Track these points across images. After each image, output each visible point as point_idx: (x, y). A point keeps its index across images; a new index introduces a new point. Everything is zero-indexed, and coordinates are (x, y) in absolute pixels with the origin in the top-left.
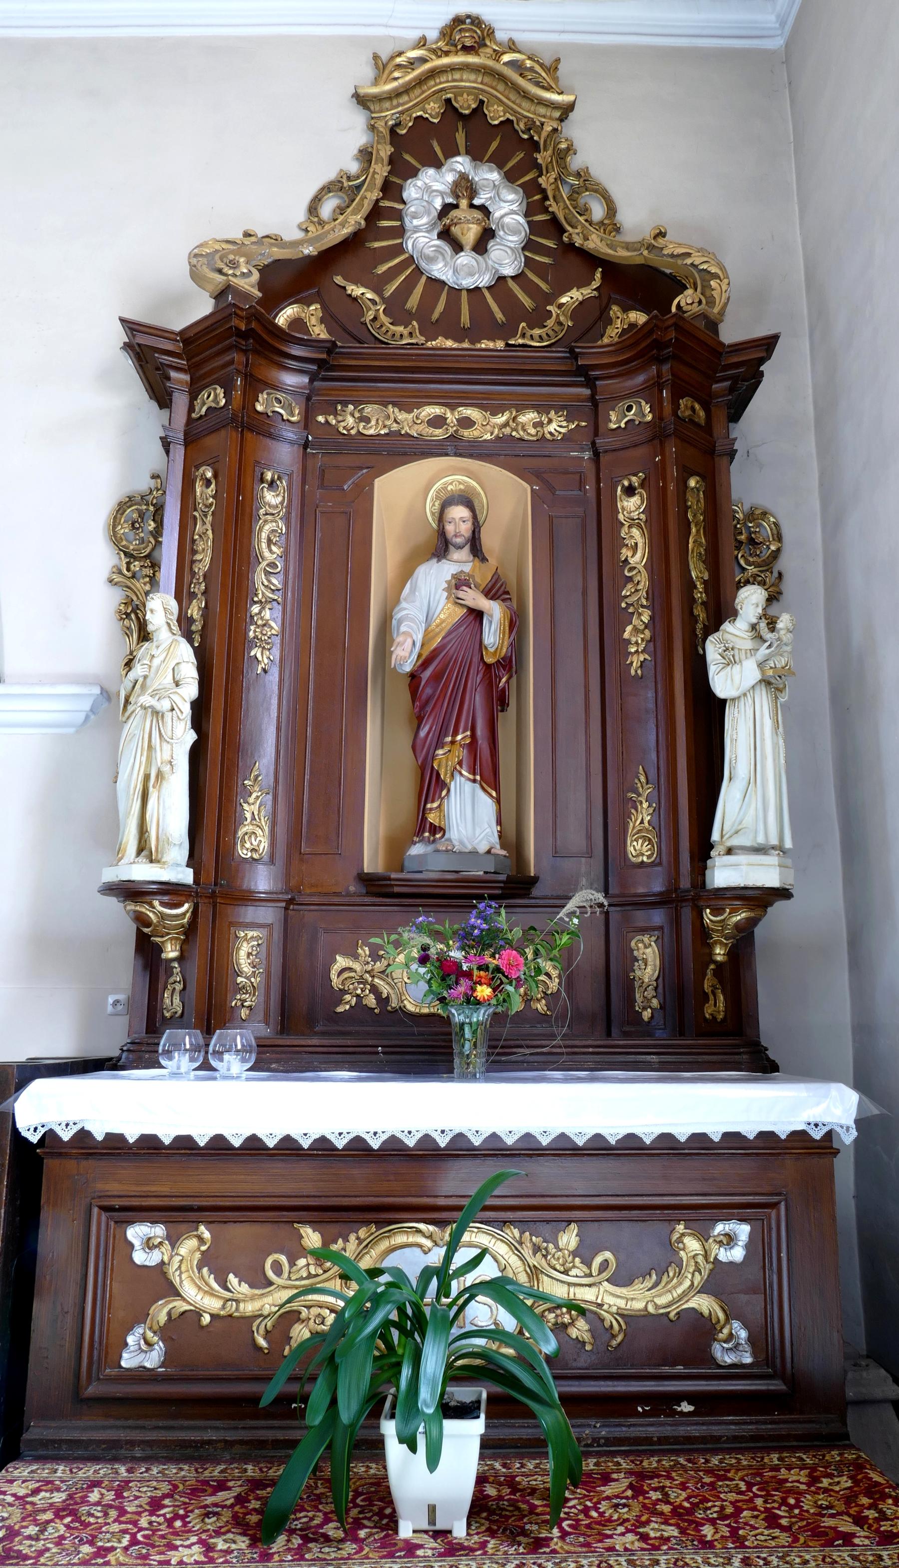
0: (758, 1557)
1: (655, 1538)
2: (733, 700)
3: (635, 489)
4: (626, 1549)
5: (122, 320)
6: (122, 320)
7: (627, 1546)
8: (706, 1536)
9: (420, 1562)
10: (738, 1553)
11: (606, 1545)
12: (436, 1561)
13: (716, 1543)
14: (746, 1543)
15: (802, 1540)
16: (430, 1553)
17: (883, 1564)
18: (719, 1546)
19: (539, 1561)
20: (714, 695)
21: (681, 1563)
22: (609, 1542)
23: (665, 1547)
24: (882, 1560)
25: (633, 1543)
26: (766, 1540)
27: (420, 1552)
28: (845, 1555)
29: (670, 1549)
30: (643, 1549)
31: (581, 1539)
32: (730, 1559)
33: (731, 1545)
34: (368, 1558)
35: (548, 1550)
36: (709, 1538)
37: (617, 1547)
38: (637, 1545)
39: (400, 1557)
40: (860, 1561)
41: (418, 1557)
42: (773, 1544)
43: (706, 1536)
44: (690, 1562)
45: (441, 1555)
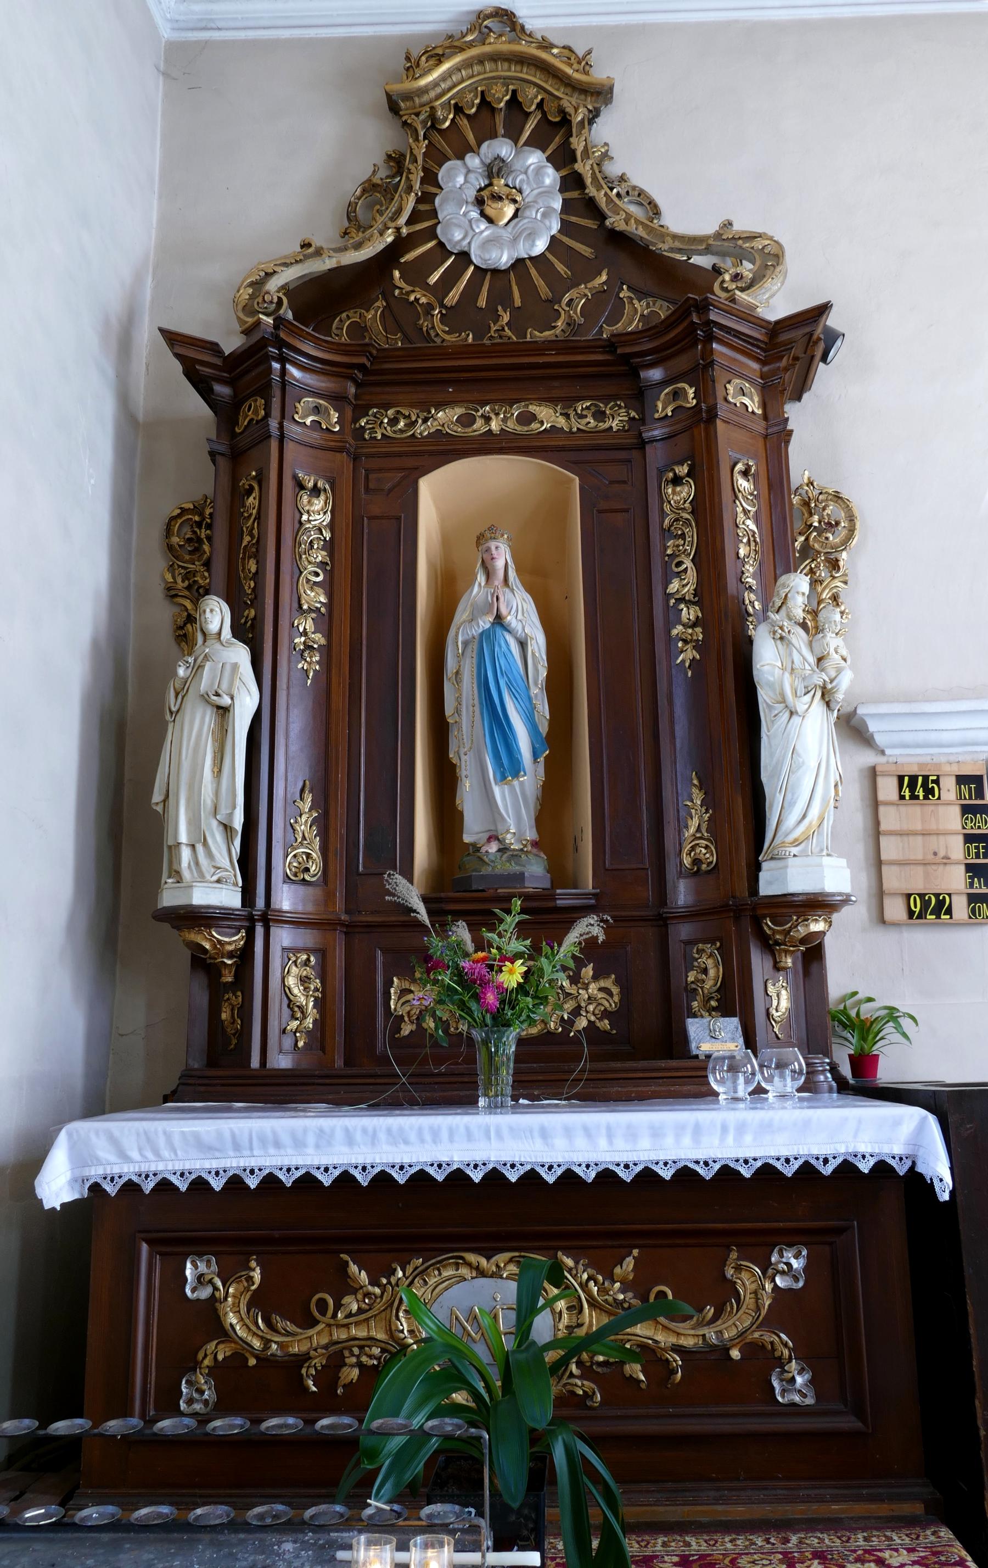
0: (773, 1544)
1: (870, 1561)
2: (465, 163)
3: (682, 478)
4: (896, 1550)
5: (161, 330)
6: (161, 330)
7: (896, 1554)
8: (819, 1563)
9: (673, 1551)
10: (791, 1548)
11: (917, 1554)
12: (660, 1551)
13: (810, 1556)
14: (781, 1557)
15: (727, 1561)
16: (666, 1558)
17: (865, 1534)
18: (807, 1554)
19: (769, 1546)
20: (510, 138)
21: (844, 1539)
22: (914, 1556)
23: (860, 1552)
24: (864, 1537)
25: (891, 1557)
26: (762, 1559)
27: (676, 1559)
28: (899, 1541)
29: (855, 1551)
30: (880, 1550)
31: (943, 1558)
32: (800, 1542)
33: (796, 1554)
34: (852, 1551)
35: (558, 1560)
36: (816, 1562)
37: (905, 1552)
38: (886, 1555)
39: (693, 1555)
40: (885, 1536)
41: (677, 1555)
42: (756, 1557)
43: (819, 1563)
44: (904, 1537)
45: (657, 1557)
